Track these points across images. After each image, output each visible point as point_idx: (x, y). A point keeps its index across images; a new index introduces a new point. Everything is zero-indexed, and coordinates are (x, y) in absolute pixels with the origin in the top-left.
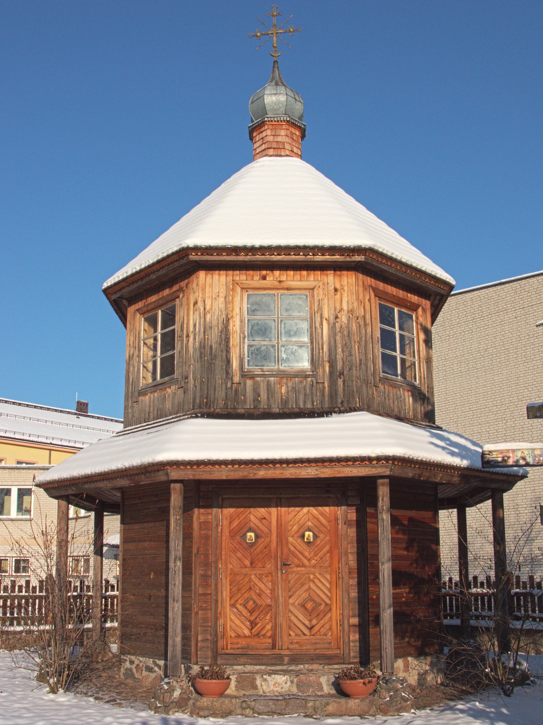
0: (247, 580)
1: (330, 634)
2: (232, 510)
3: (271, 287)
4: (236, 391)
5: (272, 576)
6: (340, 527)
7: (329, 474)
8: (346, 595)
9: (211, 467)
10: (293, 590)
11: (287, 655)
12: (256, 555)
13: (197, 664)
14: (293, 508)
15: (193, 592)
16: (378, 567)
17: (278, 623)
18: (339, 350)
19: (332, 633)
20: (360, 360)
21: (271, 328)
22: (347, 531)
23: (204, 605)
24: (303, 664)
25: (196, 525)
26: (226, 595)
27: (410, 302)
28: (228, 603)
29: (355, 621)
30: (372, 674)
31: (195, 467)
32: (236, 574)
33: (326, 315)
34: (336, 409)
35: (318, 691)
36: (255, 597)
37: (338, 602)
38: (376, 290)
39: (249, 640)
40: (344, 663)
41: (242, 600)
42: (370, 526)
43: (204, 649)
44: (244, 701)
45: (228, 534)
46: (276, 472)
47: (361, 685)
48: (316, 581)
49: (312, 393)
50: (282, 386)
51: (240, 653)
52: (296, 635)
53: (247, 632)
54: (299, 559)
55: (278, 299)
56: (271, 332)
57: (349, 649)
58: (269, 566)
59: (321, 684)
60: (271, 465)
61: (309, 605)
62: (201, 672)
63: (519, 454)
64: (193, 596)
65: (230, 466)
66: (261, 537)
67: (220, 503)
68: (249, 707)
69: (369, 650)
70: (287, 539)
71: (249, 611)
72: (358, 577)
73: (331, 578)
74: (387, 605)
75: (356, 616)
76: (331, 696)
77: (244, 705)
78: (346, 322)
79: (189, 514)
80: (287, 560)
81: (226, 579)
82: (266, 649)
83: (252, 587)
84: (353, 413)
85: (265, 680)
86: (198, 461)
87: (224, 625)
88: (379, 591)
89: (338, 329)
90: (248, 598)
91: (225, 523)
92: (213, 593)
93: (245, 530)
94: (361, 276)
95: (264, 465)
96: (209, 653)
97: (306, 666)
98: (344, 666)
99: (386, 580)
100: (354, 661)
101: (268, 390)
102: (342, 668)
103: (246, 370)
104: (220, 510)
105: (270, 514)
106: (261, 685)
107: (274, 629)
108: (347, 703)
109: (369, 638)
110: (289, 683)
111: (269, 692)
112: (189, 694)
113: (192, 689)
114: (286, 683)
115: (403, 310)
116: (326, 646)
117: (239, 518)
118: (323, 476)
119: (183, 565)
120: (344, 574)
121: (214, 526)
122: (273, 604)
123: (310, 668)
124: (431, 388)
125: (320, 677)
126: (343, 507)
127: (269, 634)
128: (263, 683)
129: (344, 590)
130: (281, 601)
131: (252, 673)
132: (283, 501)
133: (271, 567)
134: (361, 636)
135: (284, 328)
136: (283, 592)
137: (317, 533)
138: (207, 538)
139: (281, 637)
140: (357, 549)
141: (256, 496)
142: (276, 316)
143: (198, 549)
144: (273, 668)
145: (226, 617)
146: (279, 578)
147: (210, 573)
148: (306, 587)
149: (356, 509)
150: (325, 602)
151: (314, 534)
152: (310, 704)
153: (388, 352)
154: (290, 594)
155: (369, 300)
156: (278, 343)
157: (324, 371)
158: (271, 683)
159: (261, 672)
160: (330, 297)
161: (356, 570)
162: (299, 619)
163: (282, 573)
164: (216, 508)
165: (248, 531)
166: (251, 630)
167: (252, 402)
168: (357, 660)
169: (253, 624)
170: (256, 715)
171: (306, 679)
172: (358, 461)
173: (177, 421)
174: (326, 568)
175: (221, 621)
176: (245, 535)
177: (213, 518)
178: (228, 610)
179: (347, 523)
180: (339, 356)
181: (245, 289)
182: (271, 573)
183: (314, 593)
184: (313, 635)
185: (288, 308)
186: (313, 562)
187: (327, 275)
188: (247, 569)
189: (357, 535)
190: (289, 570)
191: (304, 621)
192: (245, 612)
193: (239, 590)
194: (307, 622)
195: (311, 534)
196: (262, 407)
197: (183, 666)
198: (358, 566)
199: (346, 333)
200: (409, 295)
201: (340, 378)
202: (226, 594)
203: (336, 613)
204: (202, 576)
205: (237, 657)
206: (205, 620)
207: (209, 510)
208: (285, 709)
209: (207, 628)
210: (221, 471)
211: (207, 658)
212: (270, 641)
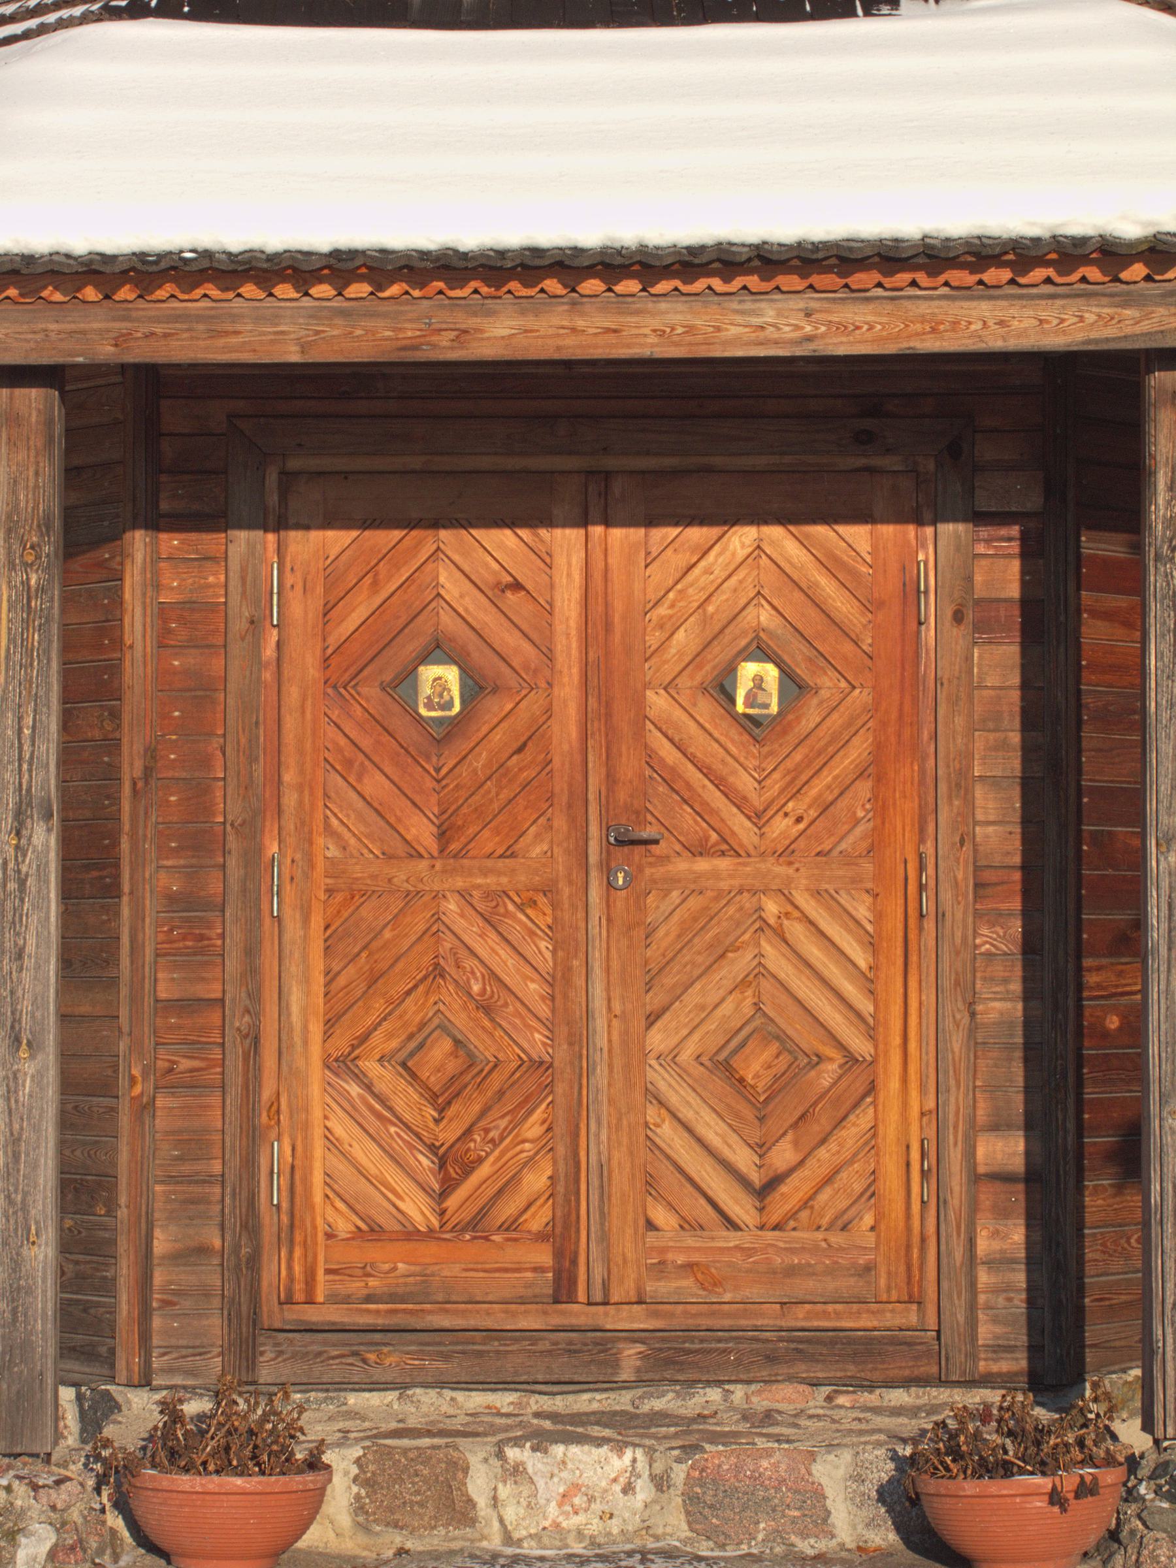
0: (419, 922)
1: (868, 1220)
2: (337, 540)
5: (555, 906)
6: (929, 634)
7: (878, 340)
8: (955, 1009)
9: (215, 293)
10: (669, 980)
11: (633, 1336)
12: (465, 788)
13: (145, 1382)
14: (673, 532)
15: (124, 991)
16: (1139, 860)
17: (590, 1157)
22: (969, 659)
23: (185, 1064)
24: (719, 1383)
25: (137, 625)
26: (304, 1010)
28: (316, 1050)
29: (1007, 1150)
30: (1094, 1444)
31: (125, 293)
32: (356, 894)
35: (804, 1536)
36: (461, 1020)
37: (913, 1045)
39: (429, 1251)
41: (390, 1036)
42: (1095, 633)
43: (187, 1304)
45: (313, 672)
47: (1040, 1503)
48: (796, 931)
51: (380, 1322)
52: (688, 1225)
53: (417, 1209)
54: (703, 812)
57: (972, 1307)
58: (537, 851)
60: (552, 285)
61: (757, 1066)
62: (168, 1430)
64: (124, 1013)
65: (323, 290)
66: (495, 690)
67: (273, 499)
69: (1080, 1310)
70: (640, 703)
71: (433, 1098)
72: (1026, 914)
73: (879, 917)
75: (1009, 1126)
79: (101, 564)
80: (640, 815)
81: (306, 920)
82: (522, 1301)
83: (451, 969)
85: (517, 1472)
86: (141, 256)
87: (296, 1175)
88: (1144, 991)
90: (422, 1026)
91: (296, 609)
92: (235, 994)
93: (411, 647)
95: (514, 285)
96: (214, 1325)
97: (739, 1392)
98: (941, 1395)
100: (995, 1368)
102: (933, 1409)
104: (271, 537)
105: (546, 560)
106: (495, 1501)
107: (567, 1189)
109: (1081, 1247)
110: (644, 1491)
112: (100, 1552)
113: (115, 1521)
114: (628, 1489)
116: (847, 1284)
117: (375, 586)
118: (841, 351)
119: (66, 842)
120: (946, 895)
121: (238, 625)
122: (562, 1054)
123: (760, 1403)
125: (812, 1456)
127: (538, 1220)
128: (504, 1492)
129: (946, 983)
130: (601, 1040)
131: (442, 1433)
132: (617, 487)
133: (550, 855)
134: (1037, 1236)
136: (616, 993)
137: (802, 671)
138: (201, 692)
139: (604, 1237)
140: (1025, 760)
143: (151, 754)
144: (559, 1404)
145: (306, 1126)
146: (595, 914)
147: (214, 886)
148: (741, 963)
149: (1024, 538)
150: (841, 1046)
151: (787, 674)
154: (654, 1000)
158: (549, 1489)
159: (492, 1430)
161: (1017, 876)
163: (610, 885)
164: (250, 527)
165: (425, 658)
166: (444, 1195)
168: (1018, 1363)
169: (452, 1166)
171: (738, 1469)
172: (1041, 262)
173: (27, 35)
174: (848, 859)
175: (279, 1152)
176: (409, 675)
177: (234, 582)
178: (315, 1090)
179: (969, 616)
182: (548, 890)
183: (783, 998)
184: (777, 1227)
186: (780, 826)
188: (423, 865)
189: (1025, 686)
190: (648, 871)
191: (727, 1153)
192: (406, 1099)
194: (743, 1159)
195: (771, 672)
197: (67, 1394)
198: (1025, 854)
202: (302, 1000)
203: (905, 1105)
204: (172, 900)
205: (363, 1345)
206: (193, 1144)
207: (210, 541)
209: (198, 1189)
210: (275, 319)
211: (201, 1351)
212: (544, 1256)
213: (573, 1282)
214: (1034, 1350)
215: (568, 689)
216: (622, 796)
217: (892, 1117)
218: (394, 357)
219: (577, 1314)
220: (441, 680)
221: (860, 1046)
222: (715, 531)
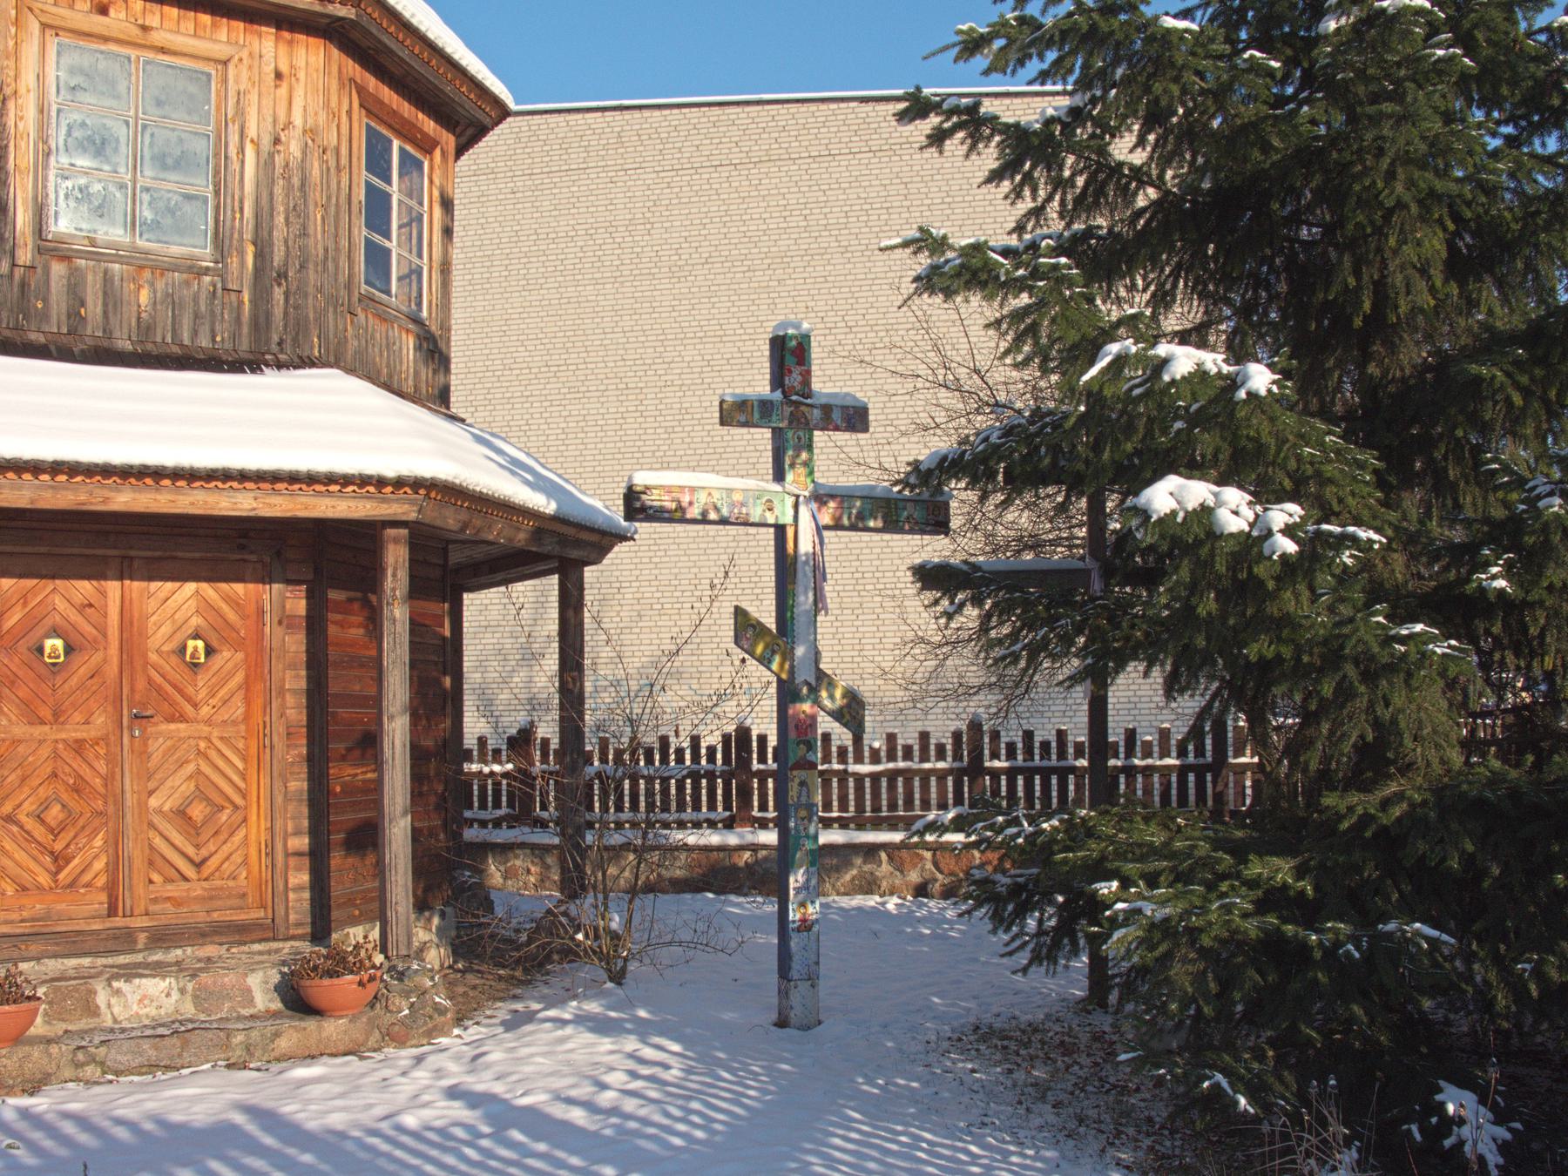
1: (244, 874)
3: (121, 36)
4: (23, 285)
5: (107, 745)
6: (267, 629)
8: (278, 785)
10: (157, 776)
11: (143, 930)
18: (280, 219)
19: (249, 873)
20: (326, 250)
21: (117, 140)
27: (421, 131)
29: (302, 843)
33: (252, 132)
34: (268, 357)
36: (65, 796)
38: (361, 90)
40: (274, 939)
44: (79, 1048)
46: (159, 497)
48: (213, 754)
49: (212, 312)
50: (140, 287)
55: (137, 69)
56: (116, 150)
59: (249, 990)
60: (149, 481)
63: (702, 498)
65: (45, 477)
68: (93, 1060)
70: (145, 656)
71: (52, 830)
74: (399, 809)
76: (275, 1015)
77: (80, 1056)
78: (298, 154)
84: (308, 371)
85: (118, 992)
89: (279, 170)
94: (335, 52)
97: (189, 950)
99: (397, 755)
101: (105, 293)
103: (50, 237)
105: (104, 594)
106: (109, 1006)
107: (113, 868)
108: (320, 1028)
110: (175, 995)
111: (128, 1019)
114: (168, 995)
115: (408, 148)
116: (235, 902)
122: (111, 809)
124: (446, 328)
126: (276, 586)
128: (113, 1001)
129: (275, 774)
132: (136, 564)
135: (151, 145)
137: (215, 644)
139: (131, 888)
141: (69, 551)
142: (132, 113)
146: (126, 749)
148: (191, 768)
150: (232, 803)
152: (239, 1038)
153: (377, 238)
154: (151, 785)
155: (349, 113)
156: (135, 182)
157: (243, 263)
158: (133, 999)
160: (263, 89)
162: (173, 845)
166: (57, 873)
167: (64, 318)
170: (110, 1077)
180: (279, 234)
181: (51, 27)
185: (163, 98)
187: (260, 36)
189: (308, 651)
192: (39, 832)
193: (24, 779)
194: (190, 851)
196: (89, 332)
199: (296, 181)
200: (420, 115)
201: (279, 285)
208: (180, 1055)
212: (104, 897)
213: (116, 909)
214: (313, 923)
215: (114, 650)
216: (137, 697)
217: (254, 830)
218: (75, 508)
219: (118, 921)
220: (54, 644)
221: (239, 800)
222: (178, 584)
